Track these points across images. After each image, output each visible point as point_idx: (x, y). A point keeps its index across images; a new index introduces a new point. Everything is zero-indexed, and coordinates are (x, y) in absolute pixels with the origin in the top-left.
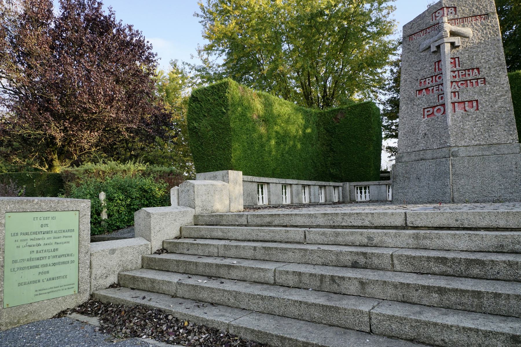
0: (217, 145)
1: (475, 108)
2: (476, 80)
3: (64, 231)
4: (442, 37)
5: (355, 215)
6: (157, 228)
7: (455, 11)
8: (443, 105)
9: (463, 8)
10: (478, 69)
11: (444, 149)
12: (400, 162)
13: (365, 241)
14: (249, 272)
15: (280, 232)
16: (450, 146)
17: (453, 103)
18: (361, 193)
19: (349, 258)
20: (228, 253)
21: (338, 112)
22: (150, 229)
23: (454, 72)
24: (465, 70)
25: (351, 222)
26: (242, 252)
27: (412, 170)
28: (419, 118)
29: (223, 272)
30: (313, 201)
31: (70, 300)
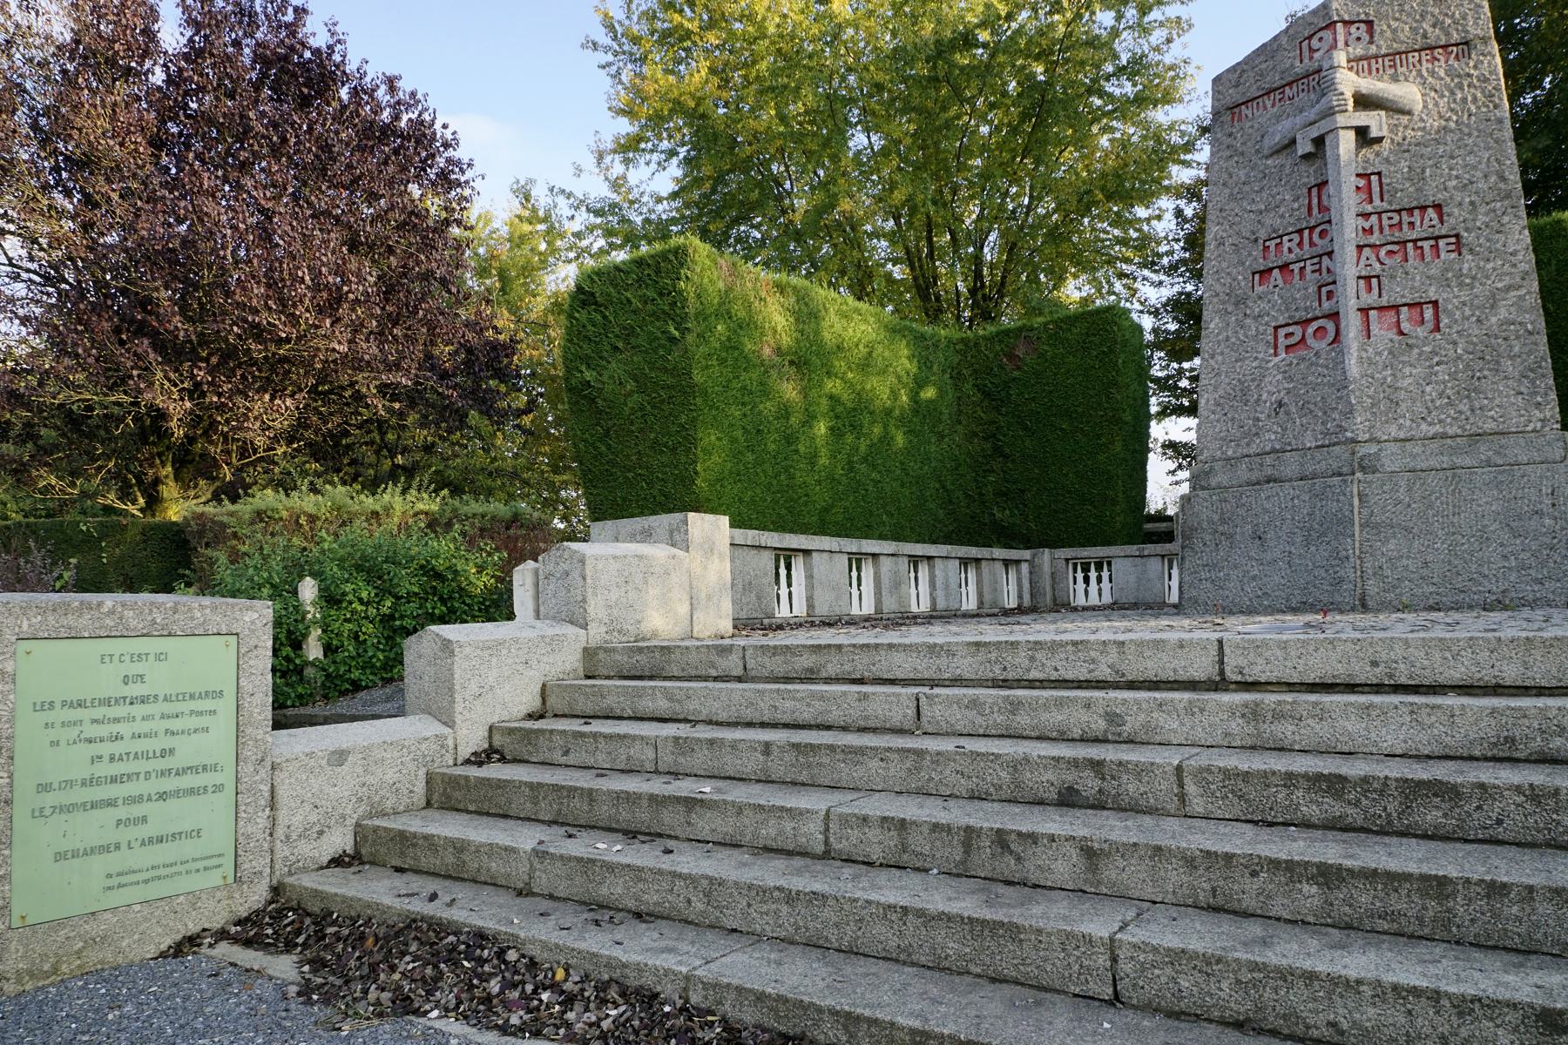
0: (652, 436)
1: (1430, 325)
2: (1432, 242)
3: (192, 697)
4: (1330, 113)
5: (1069, 647)
6: (473, 687)
7: (1371, 32)
8: (1334, 316)
9: (1394, 24)
10: (1438, 207)
11: (1337, 448)
12: (1203, 488)
13: (1099, 725)
14: (748, 819)
15: (842, 700)
16: (1354, 441)
17: (1364, 311)
18: (1087, 580)
19: (1049, 776)
20: (685, 763)
21: (1018, 337)
22: (451, 689)
23: (1366, 216)
24: (1399, 211)
25: (1056, 669)
26: (728, 759)
27: (1241, 511)
28: (1261, 356)
29: (670, 819)
30: (941, 604)
31: (212, 904)
